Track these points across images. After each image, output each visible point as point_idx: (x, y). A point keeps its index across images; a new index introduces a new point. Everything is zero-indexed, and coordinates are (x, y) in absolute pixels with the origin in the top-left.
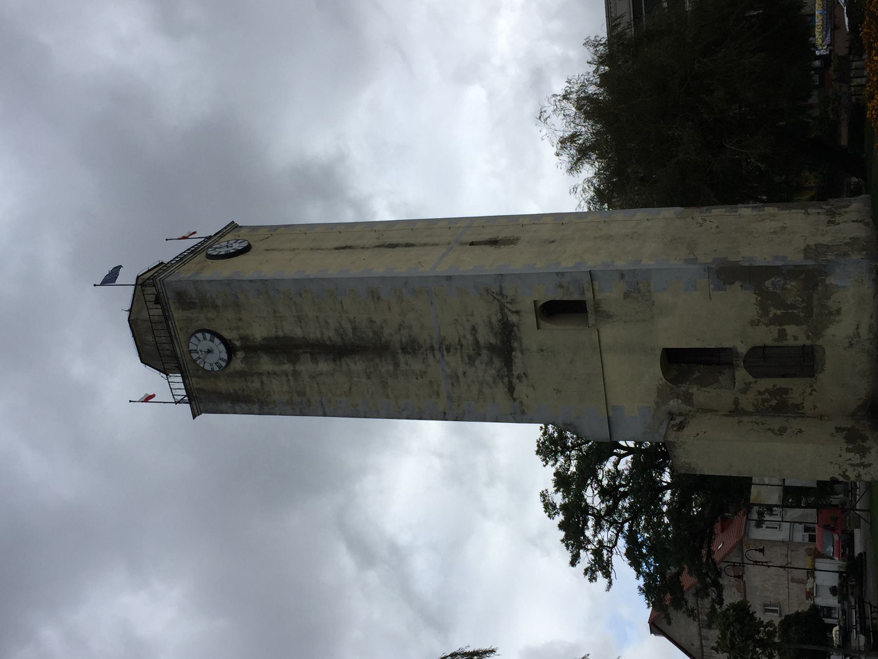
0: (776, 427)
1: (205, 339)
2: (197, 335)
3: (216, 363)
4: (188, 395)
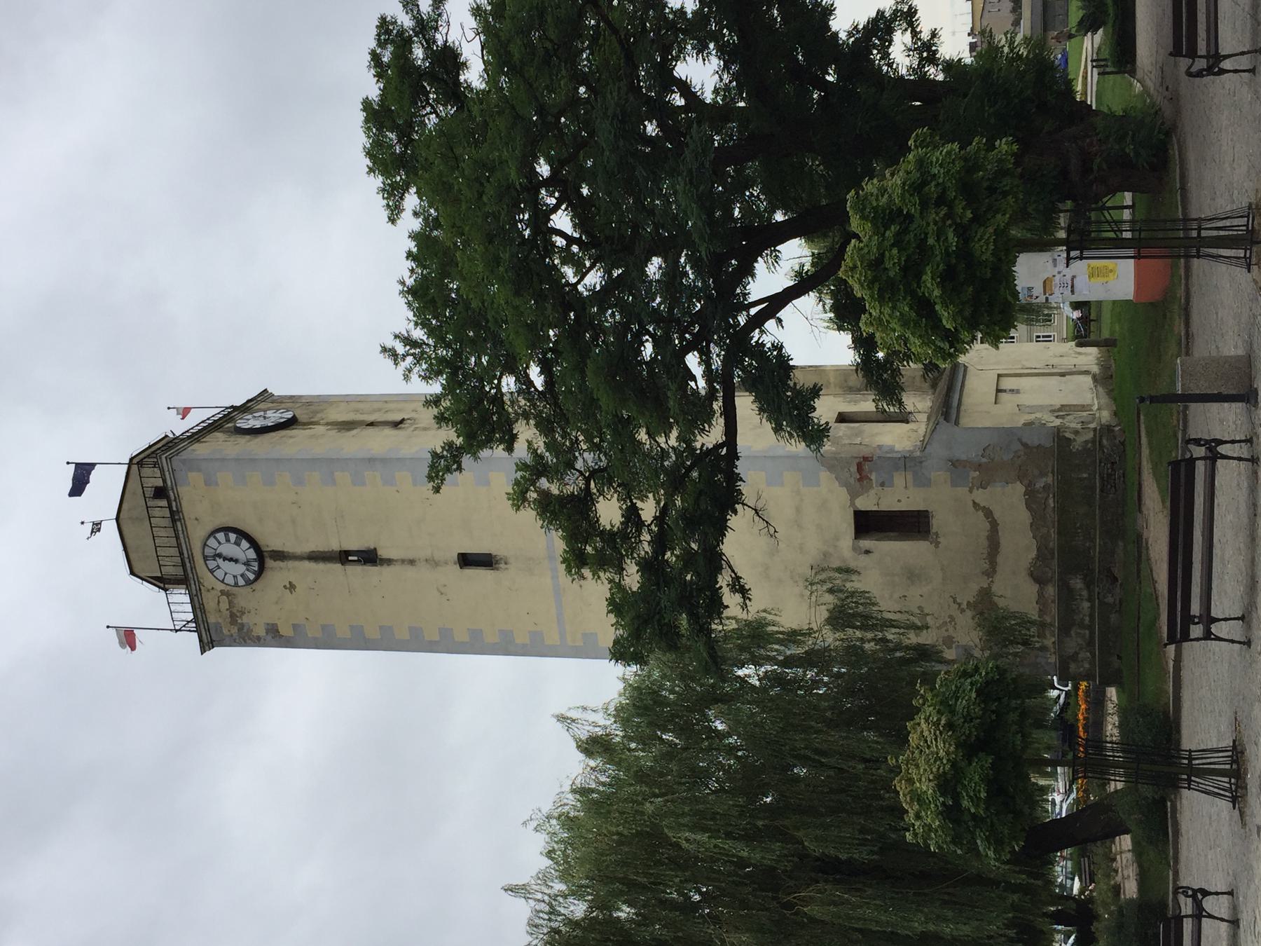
0: (738, 598)
1: (228, 540)
2: (218, 535)
3: (242, 575)
4: (195, 620)
